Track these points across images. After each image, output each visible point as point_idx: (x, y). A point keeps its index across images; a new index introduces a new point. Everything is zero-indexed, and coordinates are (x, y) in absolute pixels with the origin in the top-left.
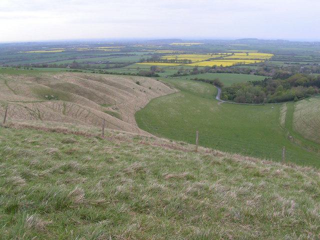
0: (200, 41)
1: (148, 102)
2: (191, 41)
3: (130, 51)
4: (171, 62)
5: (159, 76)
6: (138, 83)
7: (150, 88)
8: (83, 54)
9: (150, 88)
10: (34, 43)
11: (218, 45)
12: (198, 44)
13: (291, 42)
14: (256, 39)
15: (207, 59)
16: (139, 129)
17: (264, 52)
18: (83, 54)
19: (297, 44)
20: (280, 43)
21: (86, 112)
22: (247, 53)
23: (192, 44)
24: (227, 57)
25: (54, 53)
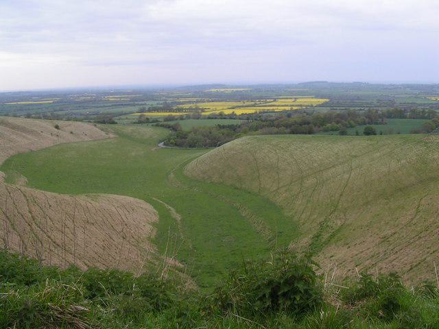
0: (249, 86)
1: (52, 145)
2: (232, 87)
3: (280, 96)
4: (179, 112)
5: (116, 123)
6: (57, 127)
7: (71, 133)
8: (78, 105)
9: (71, 133)
10: (27, 92)
11: (268, 91)
12: (242, 89)
13: (372, 85)
14: (326, 82)
15: (230, 107)
16: (38, 193)
17: (317, 97)
18: (78, 105)
19: (394, 87)
20: (334, 85)
21: (100, 314)
22: (295, 98)
23: (235, 90)
24: (267, 104)
25: (41, 104)
